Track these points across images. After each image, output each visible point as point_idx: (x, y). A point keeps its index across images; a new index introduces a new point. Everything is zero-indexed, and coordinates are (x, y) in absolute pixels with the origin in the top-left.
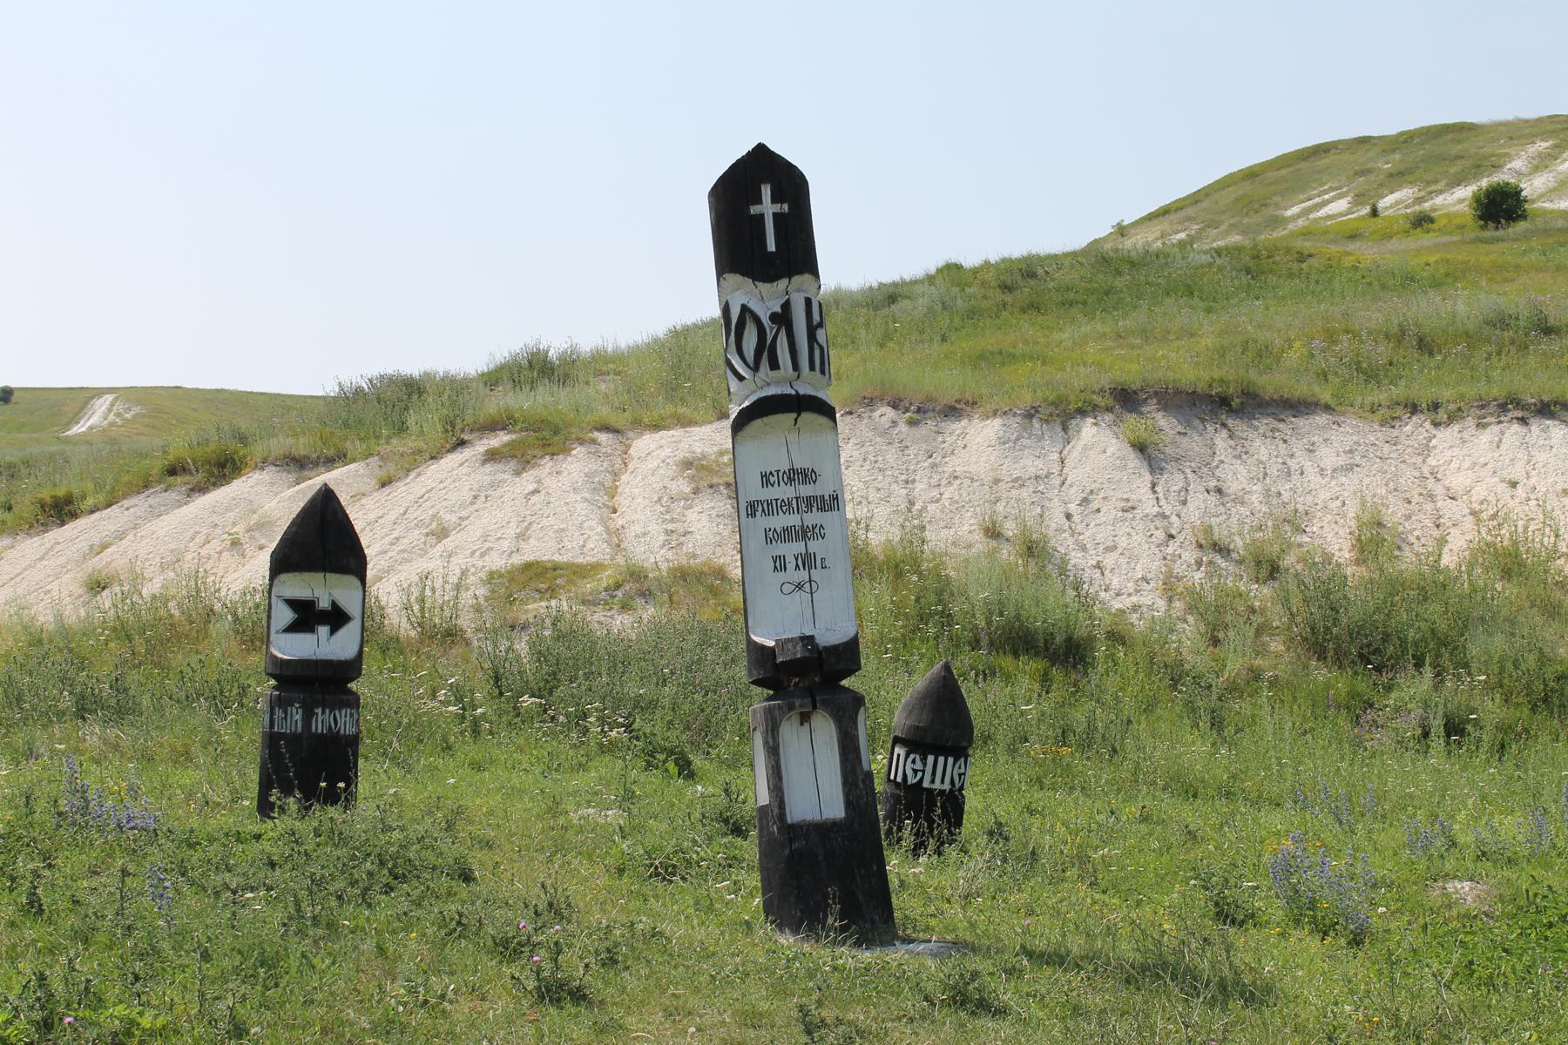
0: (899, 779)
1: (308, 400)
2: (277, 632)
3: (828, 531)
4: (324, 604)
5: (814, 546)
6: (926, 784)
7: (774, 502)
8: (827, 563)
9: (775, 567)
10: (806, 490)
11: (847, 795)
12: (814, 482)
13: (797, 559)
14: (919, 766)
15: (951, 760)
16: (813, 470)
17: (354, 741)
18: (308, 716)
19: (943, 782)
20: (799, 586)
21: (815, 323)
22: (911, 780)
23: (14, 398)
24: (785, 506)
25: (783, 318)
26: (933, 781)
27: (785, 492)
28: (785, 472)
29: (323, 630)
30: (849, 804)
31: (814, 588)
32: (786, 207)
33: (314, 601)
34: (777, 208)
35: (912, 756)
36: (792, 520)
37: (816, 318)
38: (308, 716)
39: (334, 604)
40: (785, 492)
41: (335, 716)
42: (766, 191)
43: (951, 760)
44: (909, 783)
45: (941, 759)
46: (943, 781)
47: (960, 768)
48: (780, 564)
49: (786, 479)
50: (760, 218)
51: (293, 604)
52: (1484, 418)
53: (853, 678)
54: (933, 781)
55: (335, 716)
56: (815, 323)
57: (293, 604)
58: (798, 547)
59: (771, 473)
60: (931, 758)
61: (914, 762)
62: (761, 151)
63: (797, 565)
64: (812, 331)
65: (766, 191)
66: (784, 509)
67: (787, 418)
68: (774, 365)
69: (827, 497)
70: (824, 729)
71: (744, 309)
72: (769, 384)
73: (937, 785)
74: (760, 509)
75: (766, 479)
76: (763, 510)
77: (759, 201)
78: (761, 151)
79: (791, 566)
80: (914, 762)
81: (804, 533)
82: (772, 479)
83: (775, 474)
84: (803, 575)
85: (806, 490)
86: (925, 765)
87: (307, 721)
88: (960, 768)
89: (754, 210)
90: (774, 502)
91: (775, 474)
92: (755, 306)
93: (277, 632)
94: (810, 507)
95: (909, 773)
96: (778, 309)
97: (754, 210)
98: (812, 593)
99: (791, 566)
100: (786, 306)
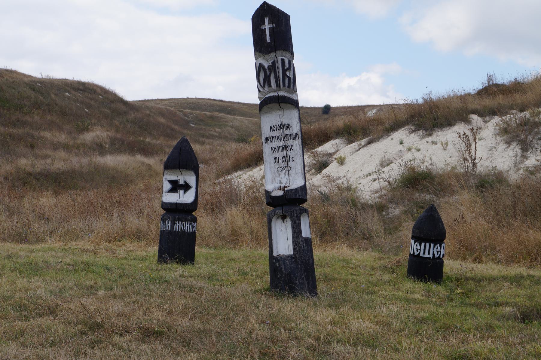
0: (412, 253)
1: (206, 100)
2: (165, 192)
3: (294, 147)
4: (182, 182)
5: (290, 153)
6: (422, 255)
7: (275, 137)
9: (275, 162)
10: (287, 132)
11: (294, 246)
12: (290, 129)
13: (283, 158)
14: (419, 247)
15: (432, 245)
16: (289, 124)
17: (192, 236)
18: (173, 224)
19: (429, 254)
20: (283, 169)
21: (286, 68)
22: (416, 253)
24: (279, 138)
25: (273, 67)
26: (424, 253)
27: (277, 133)
28: (279, 126)
29: (181, 192)
30: (294, 249)
31: (289, 169)
33: (178, 181)
34: (271, 26)
35: (416, 243)
36: (281, 143)
37: (287, 65)
38: (173, 224)
39: (185, 182)
40: (277, 133)
41: (184, 228)
43: (432, 245)
44: (415, 254)
45: (428, 245)
46: (429, 254)
47: (437, 248)
48: (276, 160)
49: (279, 128)
51: (171, 182)
52: (185, 109)
53: (303, 204)
54: (424, 253)
55: (184, 228)
56: (286, 68)
57: (171, 182)
58: (284, 153)
59: (274, 126)
60: (423, 244)
61: (417, 246)
62: (265, 3)
63: (283, 160)
64: (284, 71)
66: (278, 139)
67: (276, 105)
68: (270, 86)
69: (294, 134)
72: (270, 93)
73: (426, 255)
74: (270, 140)
75: (272, 128)
76: (271, 140)
77: (264, 23)
78: (265, 3)
79: (281, 161)
80: (417, 246)
82: (274, 129)
83: (275, 126)
85: (287, 132)
86: (420, 246)
87: (172, 227)
88: (437, 248)
89: (263, 27)
90: (275, 137)
91: (275, 126)
93: (165, 192)
95: (415, 250)
97: (263, 27)
98: (288, 171)
99: (281, 161)
100: (274, 63)
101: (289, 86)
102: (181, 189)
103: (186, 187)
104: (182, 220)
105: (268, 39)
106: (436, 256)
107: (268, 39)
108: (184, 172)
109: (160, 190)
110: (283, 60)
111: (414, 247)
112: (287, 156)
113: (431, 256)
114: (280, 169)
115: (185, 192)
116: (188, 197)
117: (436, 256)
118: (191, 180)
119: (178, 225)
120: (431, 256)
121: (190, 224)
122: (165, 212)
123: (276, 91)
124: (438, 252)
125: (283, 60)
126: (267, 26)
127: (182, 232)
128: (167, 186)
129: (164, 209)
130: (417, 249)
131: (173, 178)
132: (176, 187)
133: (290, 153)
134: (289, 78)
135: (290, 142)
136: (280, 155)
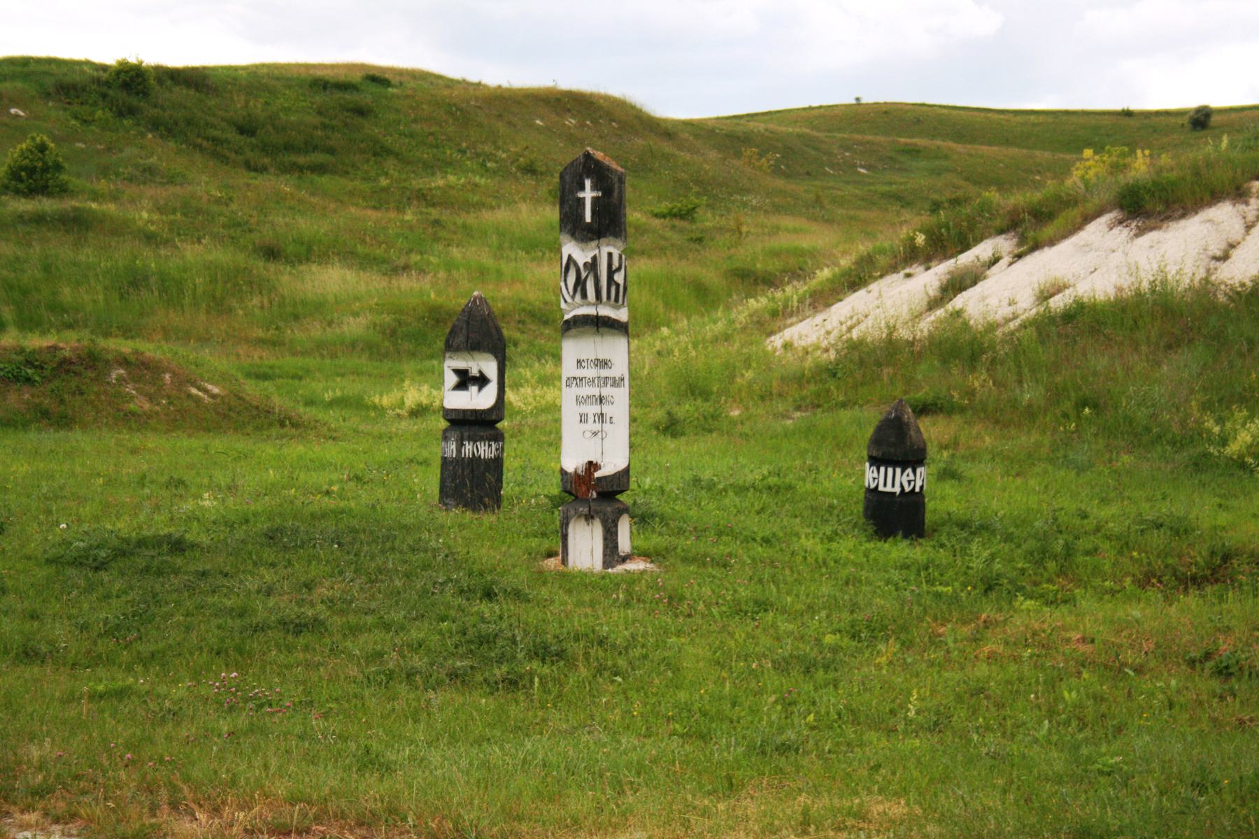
3: (616, 400)
4: (474, 372)
5: (606, 409)
6: (881, 488)
8: (614, 420)
10: (605, 373)
14: (875, 475)
15: (898, 470)
18: (460, 445)
19: (893, 485)
20: (595, 434)
22: (873, 486)
23: (1215, 119)
25: (593, 266)
26: (885, 485)
27: (591, 372)
29: (474, 389)
32: (600, 194)
36: (595, 391)
38: (460, 445)
39: (480, 372)
40: (591, 372)
42: (588, 183)
45: (890, 470)
46: (893, 485)
48: (583, 419)
50: (581, 202)
51: (457, 372)
54: (885, 485)
57: (457, 372)
58: (596, 409)
65: (588, 183)
68: (584, 296)
70: (597, 530)
71: (570, 257)
73: (889, 489)
77: (583, 188)
81: (601, 400)
84: (597, 427)
85: (605, 373)
87: (459, 451)
89: (581, 195)
92: (575, 256)
94: (605, 384)
95: (871, 480)
96: (589, 260)
100: (594, 258)
101: (617, 300)
102: (474, 385)
103: (482, 381)
104: (473, 439)
105: (588, 218)
106: (907, 489)
107: (588, 218)
108: (476, 355)
109: (439, 383)
110: (610, 255)
111: (872, 476)
112: (602, 414)
113: (897, 490)
114: (588, 434)
115: (480, 390)
116: (482, 399)
117: (907, 489)
118: (489, 367)
119: (468, 448)
120: (897, 490)
121: (490, 446)
122: (449, 424)
123: (595, 305)
124: (909, 482)
125: (610, 255)
126: (588, 194)
127: (475, 461)
128: (451, 379)
129: (449, 420)
130: (874, 479)
131: (461, 364)
132: (465, 380)
133: (606, 409)
134: (618, 285)
135: (607, 391)
136: (594, 409)
